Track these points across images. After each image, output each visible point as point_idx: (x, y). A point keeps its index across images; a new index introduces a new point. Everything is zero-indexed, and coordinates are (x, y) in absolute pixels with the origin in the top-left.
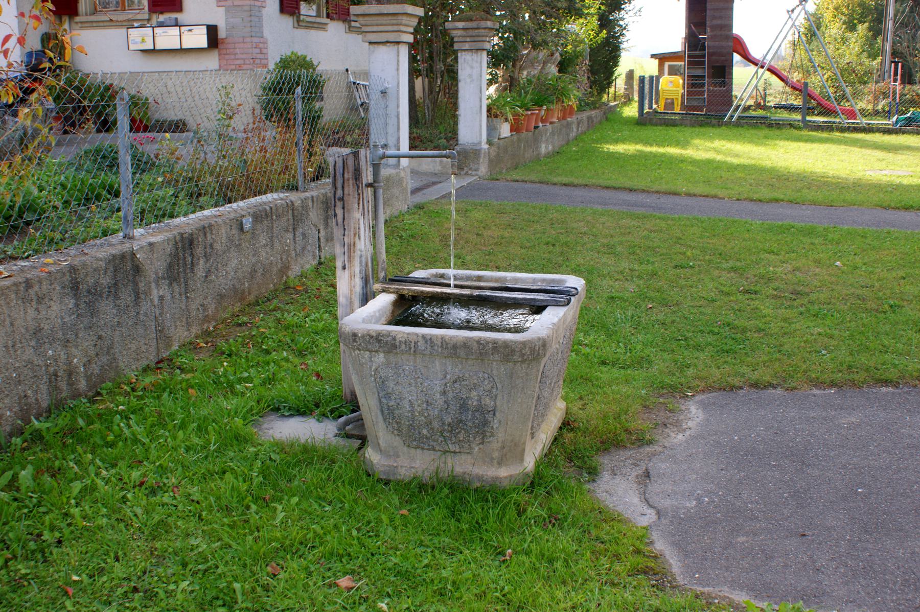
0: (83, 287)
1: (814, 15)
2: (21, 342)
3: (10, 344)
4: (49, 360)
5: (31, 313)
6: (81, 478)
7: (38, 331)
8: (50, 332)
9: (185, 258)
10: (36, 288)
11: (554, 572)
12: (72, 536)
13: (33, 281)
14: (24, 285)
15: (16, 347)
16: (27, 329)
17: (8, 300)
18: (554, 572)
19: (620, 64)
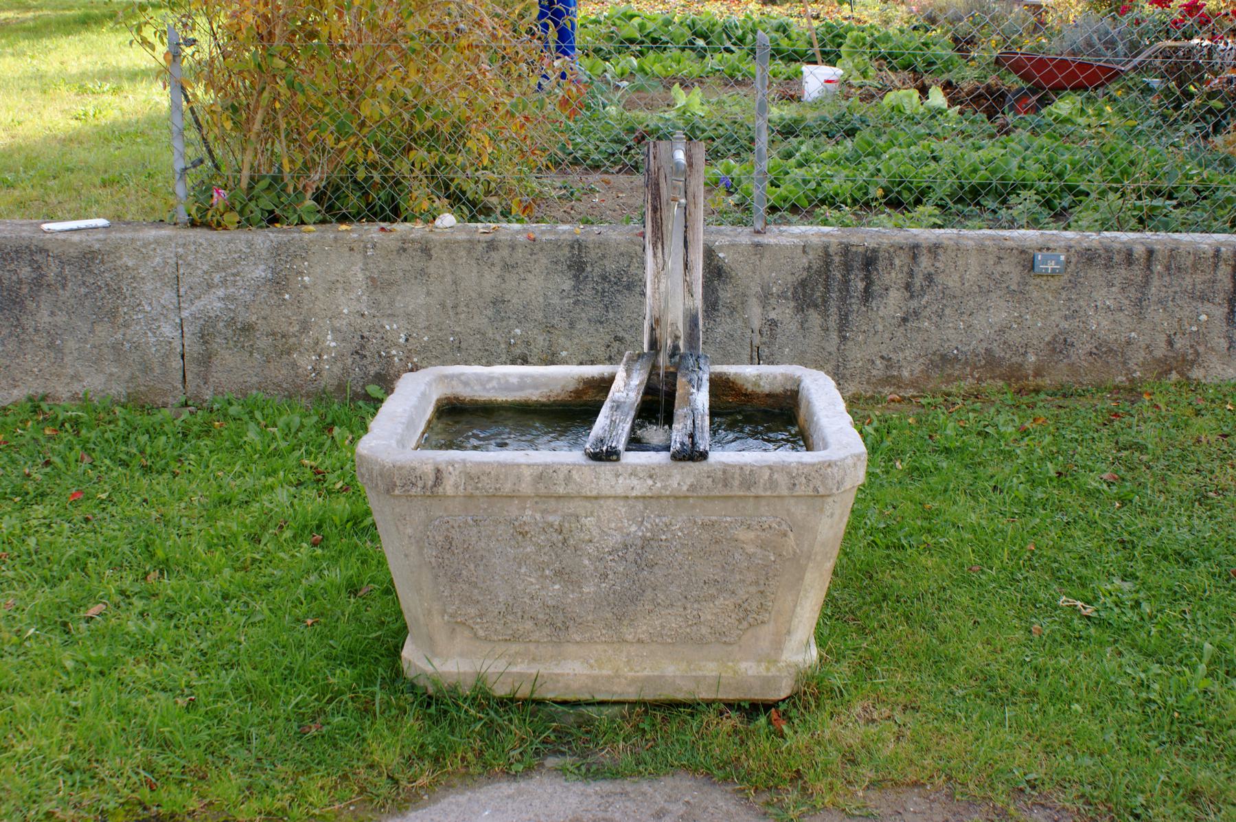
0: (593, 271)
1: (657, 316)
2: (467, 306)
3: (449, 303)
4: (514, 338)
5: (490, 278)
6: (1205, 148)
7: (498, 302)
8: (521, 308)
9: (846, 282)
10: (505, 252)
11: (735, 123)
12: (683, 588)
13: (501, 244)
14: (485, 245)
15: (459, 310)
16: (480, 295)
17: (454, 256)
18: (735, 123)
19: (396, 390)
